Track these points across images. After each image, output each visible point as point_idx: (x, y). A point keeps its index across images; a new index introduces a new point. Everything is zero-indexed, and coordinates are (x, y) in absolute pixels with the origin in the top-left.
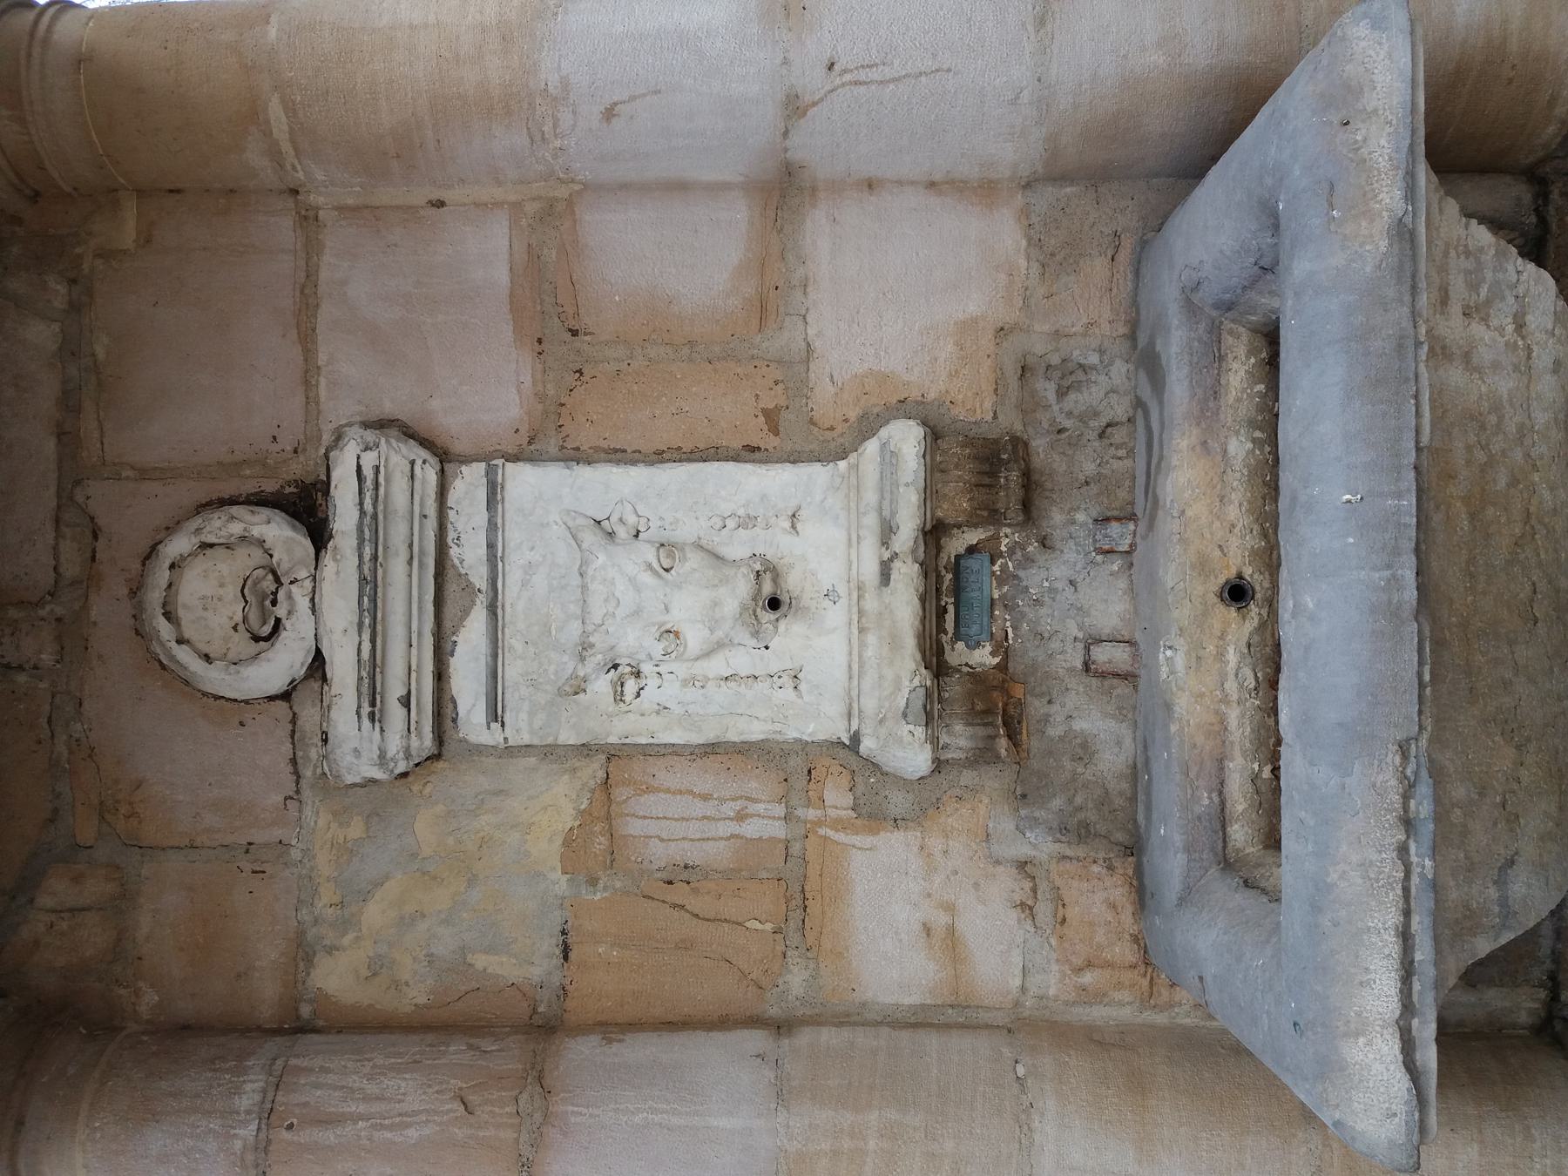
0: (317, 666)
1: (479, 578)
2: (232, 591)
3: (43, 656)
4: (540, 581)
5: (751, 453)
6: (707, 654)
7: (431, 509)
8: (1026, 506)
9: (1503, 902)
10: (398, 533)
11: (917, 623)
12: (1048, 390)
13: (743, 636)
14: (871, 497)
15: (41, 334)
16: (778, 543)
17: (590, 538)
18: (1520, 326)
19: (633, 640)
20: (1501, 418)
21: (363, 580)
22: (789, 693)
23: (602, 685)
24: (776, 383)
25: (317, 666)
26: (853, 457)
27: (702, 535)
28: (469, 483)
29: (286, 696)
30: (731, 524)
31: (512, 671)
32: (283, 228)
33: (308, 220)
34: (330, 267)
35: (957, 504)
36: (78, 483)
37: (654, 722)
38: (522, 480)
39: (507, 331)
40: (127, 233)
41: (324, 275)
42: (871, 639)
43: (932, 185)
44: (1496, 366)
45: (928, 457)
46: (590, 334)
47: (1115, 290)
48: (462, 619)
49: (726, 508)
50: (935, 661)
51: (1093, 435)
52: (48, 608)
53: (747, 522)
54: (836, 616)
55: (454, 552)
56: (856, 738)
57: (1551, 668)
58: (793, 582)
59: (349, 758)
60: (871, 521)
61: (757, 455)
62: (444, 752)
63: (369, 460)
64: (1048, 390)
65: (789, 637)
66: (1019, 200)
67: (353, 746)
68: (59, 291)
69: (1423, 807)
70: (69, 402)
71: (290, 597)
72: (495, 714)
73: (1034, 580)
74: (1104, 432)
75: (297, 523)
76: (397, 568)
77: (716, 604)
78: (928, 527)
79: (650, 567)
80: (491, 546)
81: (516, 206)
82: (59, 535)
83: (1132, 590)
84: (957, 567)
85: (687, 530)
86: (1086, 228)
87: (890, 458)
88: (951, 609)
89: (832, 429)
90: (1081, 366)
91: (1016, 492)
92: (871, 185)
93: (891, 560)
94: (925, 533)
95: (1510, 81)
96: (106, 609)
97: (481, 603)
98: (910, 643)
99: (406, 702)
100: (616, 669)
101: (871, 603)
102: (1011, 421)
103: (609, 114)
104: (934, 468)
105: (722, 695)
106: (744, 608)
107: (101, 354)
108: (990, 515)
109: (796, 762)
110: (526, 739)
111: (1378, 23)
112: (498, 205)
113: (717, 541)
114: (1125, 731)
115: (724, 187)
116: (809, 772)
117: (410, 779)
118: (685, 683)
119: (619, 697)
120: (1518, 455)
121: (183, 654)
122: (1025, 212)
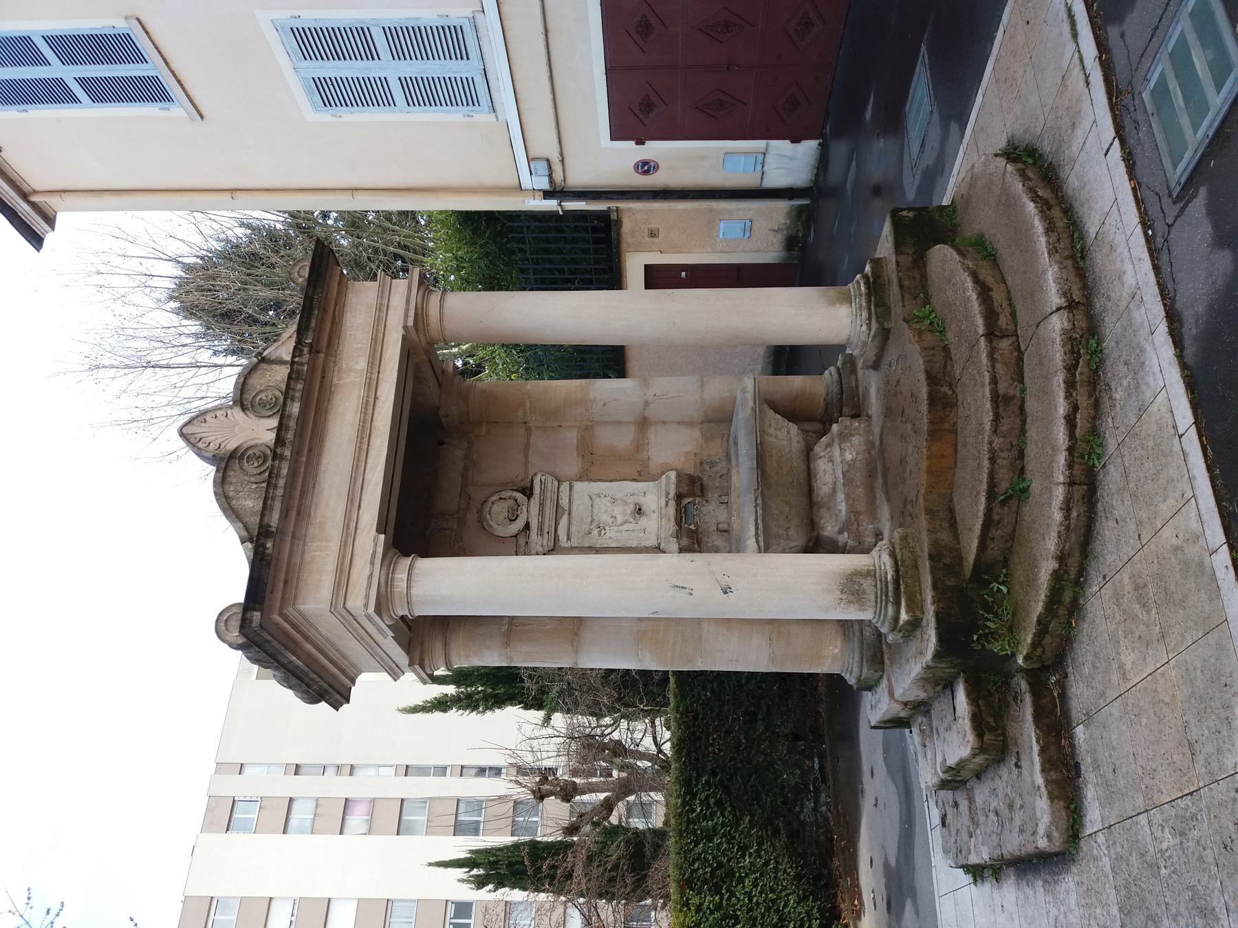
0: (527, 526)
1: (566, 508)
2: (505, 510)
4: (581, 508)
5: (634, 480)
6: (622, 525)
7: (556, 491)
8: (702, 491)
9: (787, 535)
10: (549, 495)
12: (707, 467)
13: (631, 520)
14: (664, 488)
15: (460, 453)
18: (789, 433)
19: (605, 518)
21: (540, 504)
22: (642, 534)
23: (595, 532)
25: (527, 526)
28: (565, 487)
29: (515, 536)
31: (573, 529)
32: (522, 431)
33: (528, 429)
34: (533, 439)
35: (685, 489)
36: (466, 487)
37: (609, 541)
38: (578, 486)
39: (575, 453)
40: (483, 431)
41: (531, 441)
42: (663, 520)
43: (679, 423)
44: (783, 439)
49: (628, 491)
53: (632, 495)
54: (655, 516)
55: (560, 501)
56: (659, 544)
58: (644, 508)
60: (664, 493)
63: (543, 478)
64: (707, 467)
65: (643, 522)
66: (700, 426)
68: (465, 444)
69: (759, 501)
70: (466, 469)
71: (522, 509)
73: (704, 509)
76: (548, 503)
77: (625, 510)
80: (570, 500)
81: (579, 427)
82: (460, 498)
83: (728, 513)
84: (685, 507)
85: (618, 496)
87: (668, 478)
91: (699, 487)
92: (664, 423)
96: (472, 516)
97: (566, 512)
98: (673, 519)
99: (548, 533)
101: (663, 512)
102: (698, 474)
103: (604, 405)
105: (625, 535)
106: (632, 512)
107: (475, 457)
108: (692, 494)
110: (576, 545)
111: (749, 378)
112: (574, 426)
114: (727, 545)
115: (630, 423)
118: (616, 532)
119: (600, 535)
120: (788, 456)
121: (492, 524)
122: (701, 429)
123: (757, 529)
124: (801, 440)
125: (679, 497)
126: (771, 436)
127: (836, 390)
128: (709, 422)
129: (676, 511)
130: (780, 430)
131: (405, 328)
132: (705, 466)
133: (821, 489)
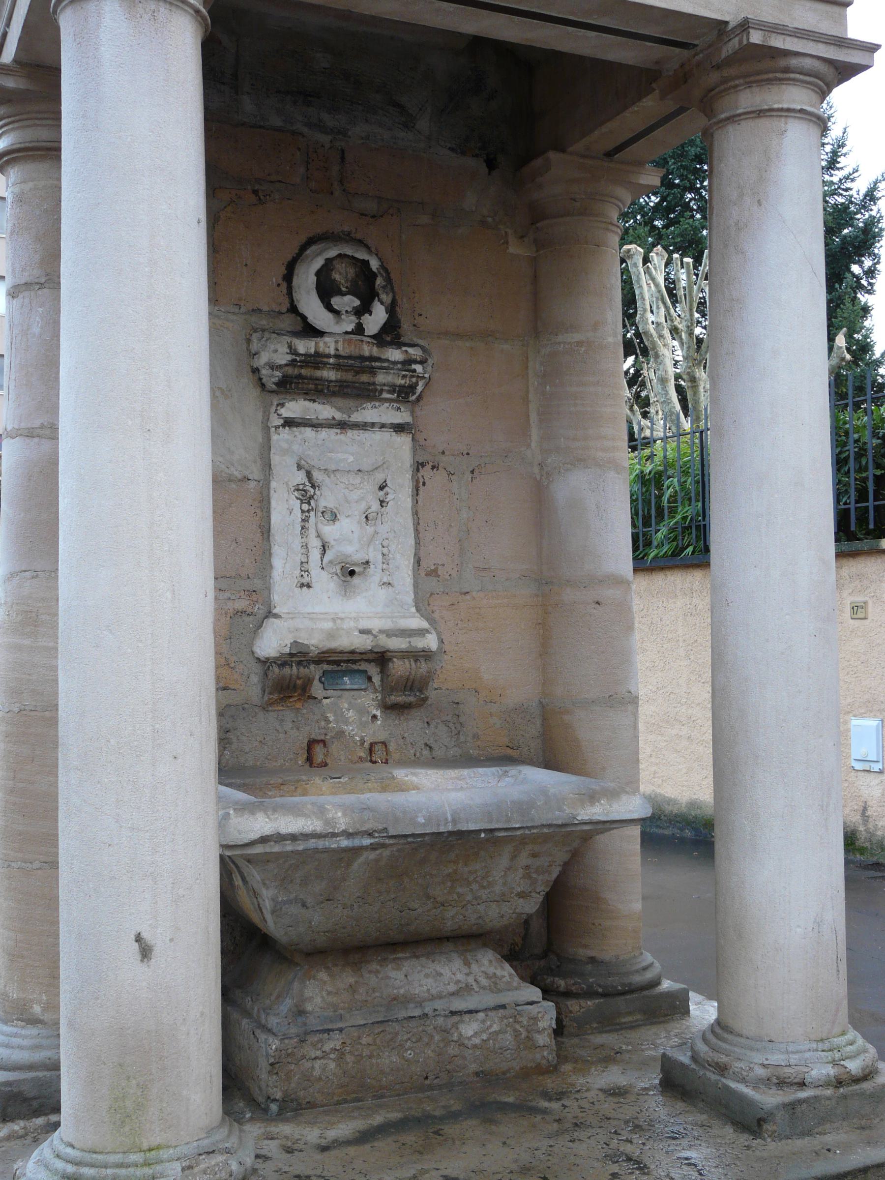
1: (357, 417)
5: (418, 562)
16: (375, 574)
17: (380, 477)
20: (484, 888)
24: (450, 575)
26: (417, 615)
27: (379, 535)
30: (385, 551)
35: (399, 668)
45: (422, 653)
46: (472, 481)
47: (493, 748)
48: (336, 407)
49: (393, 547)
56: (277, 616)
59: (272, 347)
62: (265, 393)
72: (289, 423)
74: (427, 745)
79: (369, 508)
80: (373, 425)
86: (522, 732)
88: (339, 668)
89: (429, 605)
90: (459, 732)
93: (372, 634)
95: (593, 924)
100: (312, 487)
109: (258, 584)
116: (254, 591)
120: (469, 897)
123: (293, 837)
124: (505, 921)
125: (382, 658)
126: (513, 858)
127: (614, 981)
128: (544, 719)
129: (352, 652)
130: (527, 876)
131: (745, 26)
132: (874, 708)
133: (399, 969)
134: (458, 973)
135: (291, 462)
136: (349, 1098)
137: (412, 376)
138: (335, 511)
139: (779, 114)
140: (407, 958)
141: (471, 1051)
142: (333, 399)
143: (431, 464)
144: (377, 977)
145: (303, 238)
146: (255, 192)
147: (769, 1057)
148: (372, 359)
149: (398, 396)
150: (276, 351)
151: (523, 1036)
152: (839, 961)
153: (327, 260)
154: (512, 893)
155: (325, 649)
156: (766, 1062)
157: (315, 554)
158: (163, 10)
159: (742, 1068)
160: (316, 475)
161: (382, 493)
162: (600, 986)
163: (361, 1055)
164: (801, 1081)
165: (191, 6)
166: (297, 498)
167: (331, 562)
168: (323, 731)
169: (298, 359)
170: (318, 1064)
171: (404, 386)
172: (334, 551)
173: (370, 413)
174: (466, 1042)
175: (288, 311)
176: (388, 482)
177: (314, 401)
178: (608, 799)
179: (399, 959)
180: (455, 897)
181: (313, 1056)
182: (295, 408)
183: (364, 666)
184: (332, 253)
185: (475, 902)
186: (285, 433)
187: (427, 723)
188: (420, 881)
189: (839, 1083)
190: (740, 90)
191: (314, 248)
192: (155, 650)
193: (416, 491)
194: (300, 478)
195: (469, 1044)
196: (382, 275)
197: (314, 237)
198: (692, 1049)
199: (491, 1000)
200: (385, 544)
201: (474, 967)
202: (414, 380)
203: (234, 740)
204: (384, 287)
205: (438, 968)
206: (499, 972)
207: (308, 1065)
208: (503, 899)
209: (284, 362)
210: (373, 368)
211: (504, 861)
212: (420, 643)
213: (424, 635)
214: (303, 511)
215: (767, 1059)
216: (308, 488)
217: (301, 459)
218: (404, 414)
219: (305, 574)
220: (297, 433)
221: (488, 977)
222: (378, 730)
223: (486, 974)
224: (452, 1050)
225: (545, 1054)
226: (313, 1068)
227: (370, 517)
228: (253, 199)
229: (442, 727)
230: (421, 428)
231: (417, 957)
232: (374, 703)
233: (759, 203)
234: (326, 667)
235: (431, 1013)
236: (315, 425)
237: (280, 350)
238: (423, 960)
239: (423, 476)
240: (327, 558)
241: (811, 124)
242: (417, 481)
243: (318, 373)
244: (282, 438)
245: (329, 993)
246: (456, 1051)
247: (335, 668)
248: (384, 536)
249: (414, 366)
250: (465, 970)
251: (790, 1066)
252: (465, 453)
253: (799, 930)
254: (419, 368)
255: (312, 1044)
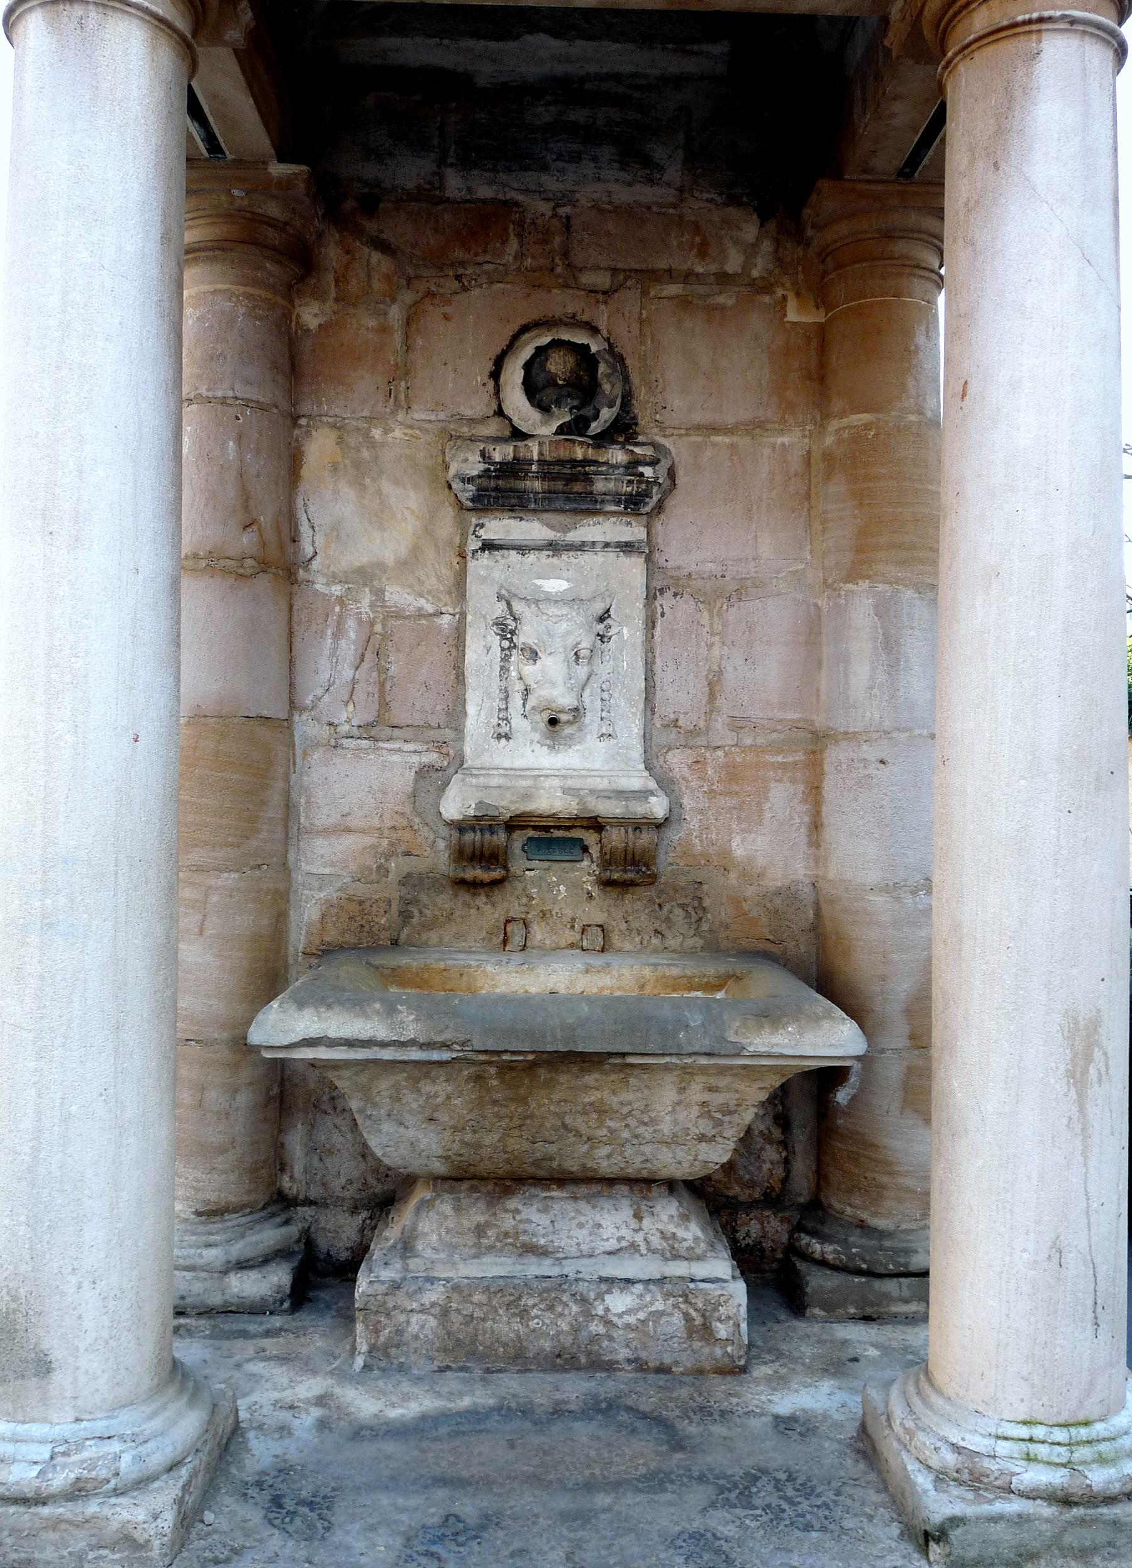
1: (574, 536)
3: (529, 260)
11: (540, 812)
17: (598, 607)
20: (646, 1124)
30: (606, 696)
35: (615, 837)
50: (514, 824)
51: (656, 926)
52: (560, 262)
57: (507, 1152)
61: (649, 713)
67: (545, 660)
72: (489, 546)
75: (608, 424)
78: (600, 820)
88: (548, 835)
90: (701, 919)
94: (596, 818)
104: (638, 825)
108: (608, 860)
109: (449, 734)
113: (595, 684)
117: (447, 490)
120: (626, 1134)
133: (545, 1210)
134: (624, 1226)
135: (491, 592)
136: (454, 1366)
137: (639, 482)
138: (535, 647)
139: (1027, 28)
140: (561, 1199)
141: (621, 1332)
142: (545, 516)
143: (673, 590)
144: (514, 1218)
145: (514, 327)
146: (458, 278)
147: (967, 1436)
148: (586, 462)
149: (626, 508)
150: (466, 460)
151: (697, 1323)
152: (1099, 1310)
153: (537, 348)
154: (688, 1135)
155: (518, 812)
156: (962, 1444)
157: (517, 700)
158: (93, 15)
159: (925, 1444)
160: (518, 607)
161: (602, 626)
162: (865, 1261)
163: (472, 1316)
164: (1006, 1486)
165: (138, 7)
166: (497, 634)
167: (533, 708)
168: (523, 909)
169: (492, 468)
170: (414, 1319)
171: (631, 495)
172: (536, 695)
173: (592, 530)
174: (615, 1319)
175: (495, 413)
176: (612, 612)
177: (521, 519)
178: (799, 1026)
179: (552, 1198)
180: (605, 1132)
181: (409, 1308)
182: (498, 527)
183: (576, 834)
184: (545, 340)
185: (635, 1141)
186: (485, 559)
187: (660, 905)
188: (552, 1108)
189: (1066, 1501)
190: (974, 9)
191: (526, 336)
192: (49, 806)
193: (650, 624)
194: (500, 609)
195: (619, 1322)
196: (606, 362)
197: (529, 324)
198: (210, 1561)
199: (652, 1268)
200: (604, 687)
201: (647, 1222)
202: (644, 486)
203: (416, 913)
204: (608, 376)
205: (598, 1218)
206: (681, 1233)
207: (402, 1318)
208: (672, 1142)
209: (475, 473)
210: (587, 474)
211: (669, 1094)
212: (639, 809)
213: (646, 798)
214: (503, 649)
215: (963, 1439)
216: (509, 622)
217: (502, 587)
218: (636, 530)
219: (503, 723)
220: (499, 558)
221: (663, 1235)
222: (595, 913)
223: (662, 1233)
224: (596, 1328)
225: (729, 1349)
226: (408, 1322)
227: (582, 653)
228: (456, 285)
229: (679, 912)
230: (661, 547)
231: (575, 1198)
232: (590, 878)
233: (996, 166)
234: (531, 833)
235: (572, 1276)
236: (522, 549)
237: (471, 459)
238: (582, 1205)
239: (661, 605)
240: (528, 707)
241: (1087, 38)
242: (654, 613)
243: (521, 485)
244: (480, 565)
245: (448, 1231)
246: (601, 1330)
247: (543, 834)
248: (604, 678)
249: (641, 469)
250: (634, 1224)
251: (994, 1457)
252: (719, 575)
253: (1025, 1255)
254: (648, 471)
255: (407, 1293)
